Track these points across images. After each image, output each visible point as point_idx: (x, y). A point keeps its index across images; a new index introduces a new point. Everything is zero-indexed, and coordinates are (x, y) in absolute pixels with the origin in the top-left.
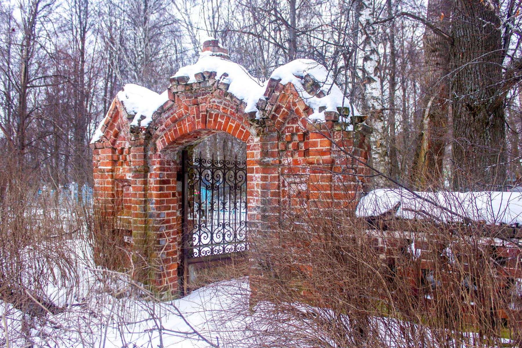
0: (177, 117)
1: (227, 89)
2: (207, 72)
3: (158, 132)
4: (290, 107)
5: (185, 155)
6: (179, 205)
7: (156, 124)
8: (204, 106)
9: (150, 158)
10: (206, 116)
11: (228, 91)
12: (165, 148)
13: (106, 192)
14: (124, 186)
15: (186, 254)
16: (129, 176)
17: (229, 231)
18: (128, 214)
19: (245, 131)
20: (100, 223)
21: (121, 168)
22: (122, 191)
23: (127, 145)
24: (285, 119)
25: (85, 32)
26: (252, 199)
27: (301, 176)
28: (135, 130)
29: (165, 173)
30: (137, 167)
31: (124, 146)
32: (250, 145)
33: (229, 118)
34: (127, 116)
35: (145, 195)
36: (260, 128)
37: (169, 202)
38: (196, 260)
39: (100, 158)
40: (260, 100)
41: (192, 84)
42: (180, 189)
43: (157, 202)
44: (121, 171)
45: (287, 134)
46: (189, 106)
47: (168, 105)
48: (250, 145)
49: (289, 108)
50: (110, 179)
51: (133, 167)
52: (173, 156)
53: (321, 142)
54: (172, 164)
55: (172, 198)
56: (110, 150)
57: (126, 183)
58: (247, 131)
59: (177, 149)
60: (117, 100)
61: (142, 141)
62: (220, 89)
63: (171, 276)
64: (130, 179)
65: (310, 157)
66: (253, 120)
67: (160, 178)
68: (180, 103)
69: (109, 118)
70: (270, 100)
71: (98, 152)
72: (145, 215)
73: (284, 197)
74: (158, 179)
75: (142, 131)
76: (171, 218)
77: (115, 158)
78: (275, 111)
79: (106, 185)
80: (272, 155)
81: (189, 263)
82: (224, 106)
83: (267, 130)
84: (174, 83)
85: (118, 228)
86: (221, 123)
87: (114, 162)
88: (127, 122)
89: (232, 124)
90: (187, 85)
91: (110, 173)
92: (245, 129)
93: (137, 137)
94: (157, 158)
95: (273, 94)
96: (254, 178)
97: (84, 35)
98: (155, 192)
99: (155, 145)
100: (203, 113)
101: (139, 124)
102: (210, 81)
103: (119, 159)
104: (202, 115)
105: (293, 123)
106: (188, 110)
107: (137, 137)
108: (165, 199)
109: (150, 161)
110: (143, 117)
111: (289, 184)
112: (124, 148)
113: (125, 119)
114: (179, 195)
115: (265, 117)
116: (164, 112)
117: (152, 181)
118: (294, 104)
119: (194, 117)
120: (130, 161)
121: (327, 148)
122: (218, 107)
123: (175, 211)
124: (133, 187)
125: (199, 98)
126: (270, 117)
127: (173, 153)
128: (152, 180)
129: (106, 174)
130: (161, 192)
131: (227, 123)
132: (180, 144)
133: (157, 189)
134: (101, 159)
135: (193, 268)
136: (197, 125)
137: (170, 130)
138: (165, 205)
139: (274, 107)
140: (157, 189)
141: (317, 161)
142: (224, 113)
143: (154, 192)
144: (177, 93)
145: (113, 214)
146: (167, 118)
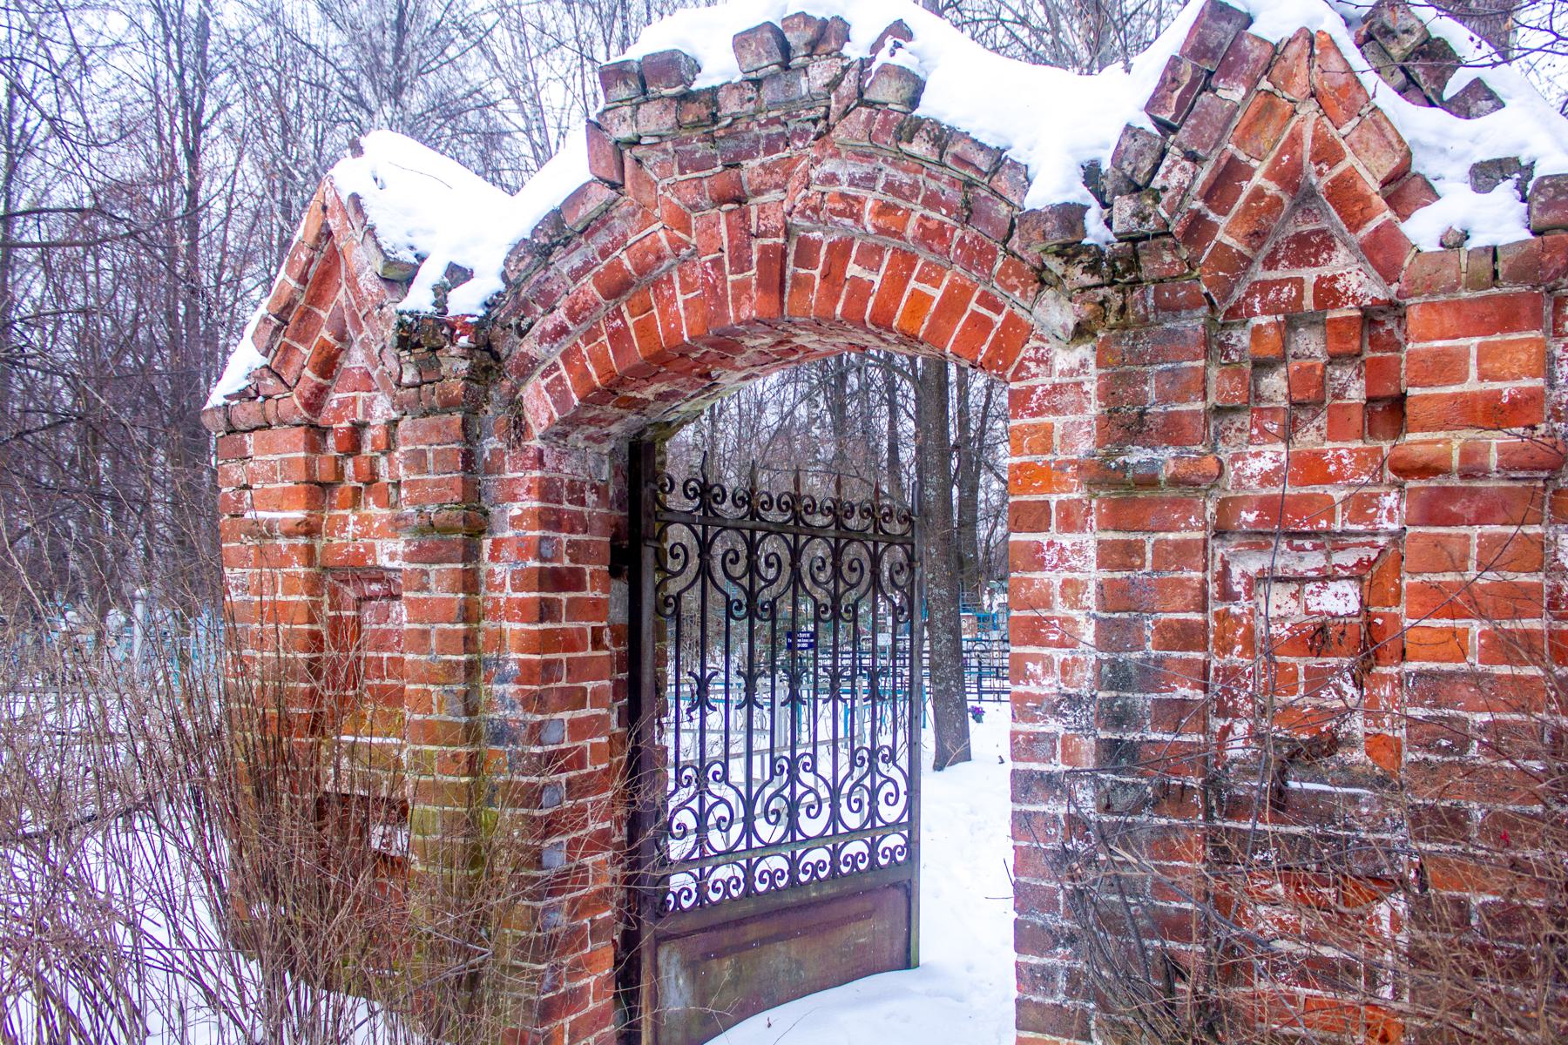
0: (627, 264)
1: (914, 102)
2: (806, 18)
3: (530, 346)
4: (1297, 168)
5: (640, 461)
6: (617, 683)
7: (524, 307)
8: (769, 208)
9: (493, 468)
10: (784, 255)
11: (916, 113)
12: (564, 421)
13: (283, 627)
14: (363, 599)
15: (641, 899)
16: (390, 552)
17: (811, 790)
18: (391, 724)
19: (999, 319)
20: (254, 772)
21: (353, 518)
22: (358, 621)
23: (382, 409)
24: (1257, 236)
25: (199, 129)
26: (1035, 658)
27: (1337, 541)
28: (418, 337)
29: (564, 537)
30: (431, 508)
31: (367, 413)
32: (1032, 390)
33: (909, 259)
34: (379, 266)
35: (469, 641)
36: (1107, 291)
37: (578, 669)
38: (687, 923)
39: (252, 471)
40: (1130, 131)
41: (714, 91)
42: (619, 614)
43: (528, 673)
44: (351, 528)
45: (1263, 320)
46: (695, 207)
47: (590, 207)
48: (1032, 390)
49: (1289, 177)
50: (300, 570)
51: (411, 510)
52: (592, 463)
53: (1484, 353)
54: (591, 497)
55: (589, 652)
56: (300, 433)
57: (375, 587)
58: (1012, 320)
59: (615, 429)
60: (330, 196)
61: (456, 387)
62: (870, 104)
63: (591, 1005)
64: (395, 565)
65: (1410, 437)
66: (1070, 251)
67: (543, 559)
68: (647, 198)
69: (293, 284)
70: (1183, 134)
71: (243, 448)
72: (471, 733)
73: (1226, 648)
74: (533, 563)
75: (452, 339)
76: (587, 743)
77: (324, 472)
78: (1208, 195)
79: (280, 597)
80: (1173, 431)
81: (660, 940)
82: (889, 198)
83: (1144, 301)
84: (621, 92)
85: (345, 790)
86: (861, 289)
87: (319, 490)
88: (381, 295)
89: (926, 288)
90: (686, 98)
91: (302, 541)
92: (998, 309)
93: (429, 368)
94: (525, 468)
95: (1205, 97)
96: (1051, 556)
97: (197, 141)
98: (518, 626)
99: (515, 404)
100: (768, 241)
101: (441, 304)
102: (813, 71)
103: (340, 474)
104: (764, 250)
105: (1299, 260)
106: (688, 231)
107: (429, 368)
108: (563, 656)
109: (490, 483)
110: (458, 274)
111: (1255, 582)
112: (365, 425)
113: (368, 282)
114: (616, 641)
115: (1151, 226)
116: (568, 240)
117: (503, 574)
118: (1327, 152)
119: (717, 263)
120: (397, 485)
121: (1527, 383)
122: (851, 206)
123: (603, 711)
124: (411, 603)
125: (750, 164)
126: (1175, 227)
127: (596, 448)
128: (502, 570)
129: (283, 542)
130: (547, 625)
131: (896, 283)
132: (631, 404)
133: (525, 611)
134: (253, 475)
135: (675, 958)
136: (736, 300)
137: (591, 336)
138: (563, 684)
139: (1204, 174)
140: (525, 611)
141: (1466, 455)
142: (881, 231)
143: (513, 627)
144: (635, 143)
145: (315, 725)
146: (576, 275)
